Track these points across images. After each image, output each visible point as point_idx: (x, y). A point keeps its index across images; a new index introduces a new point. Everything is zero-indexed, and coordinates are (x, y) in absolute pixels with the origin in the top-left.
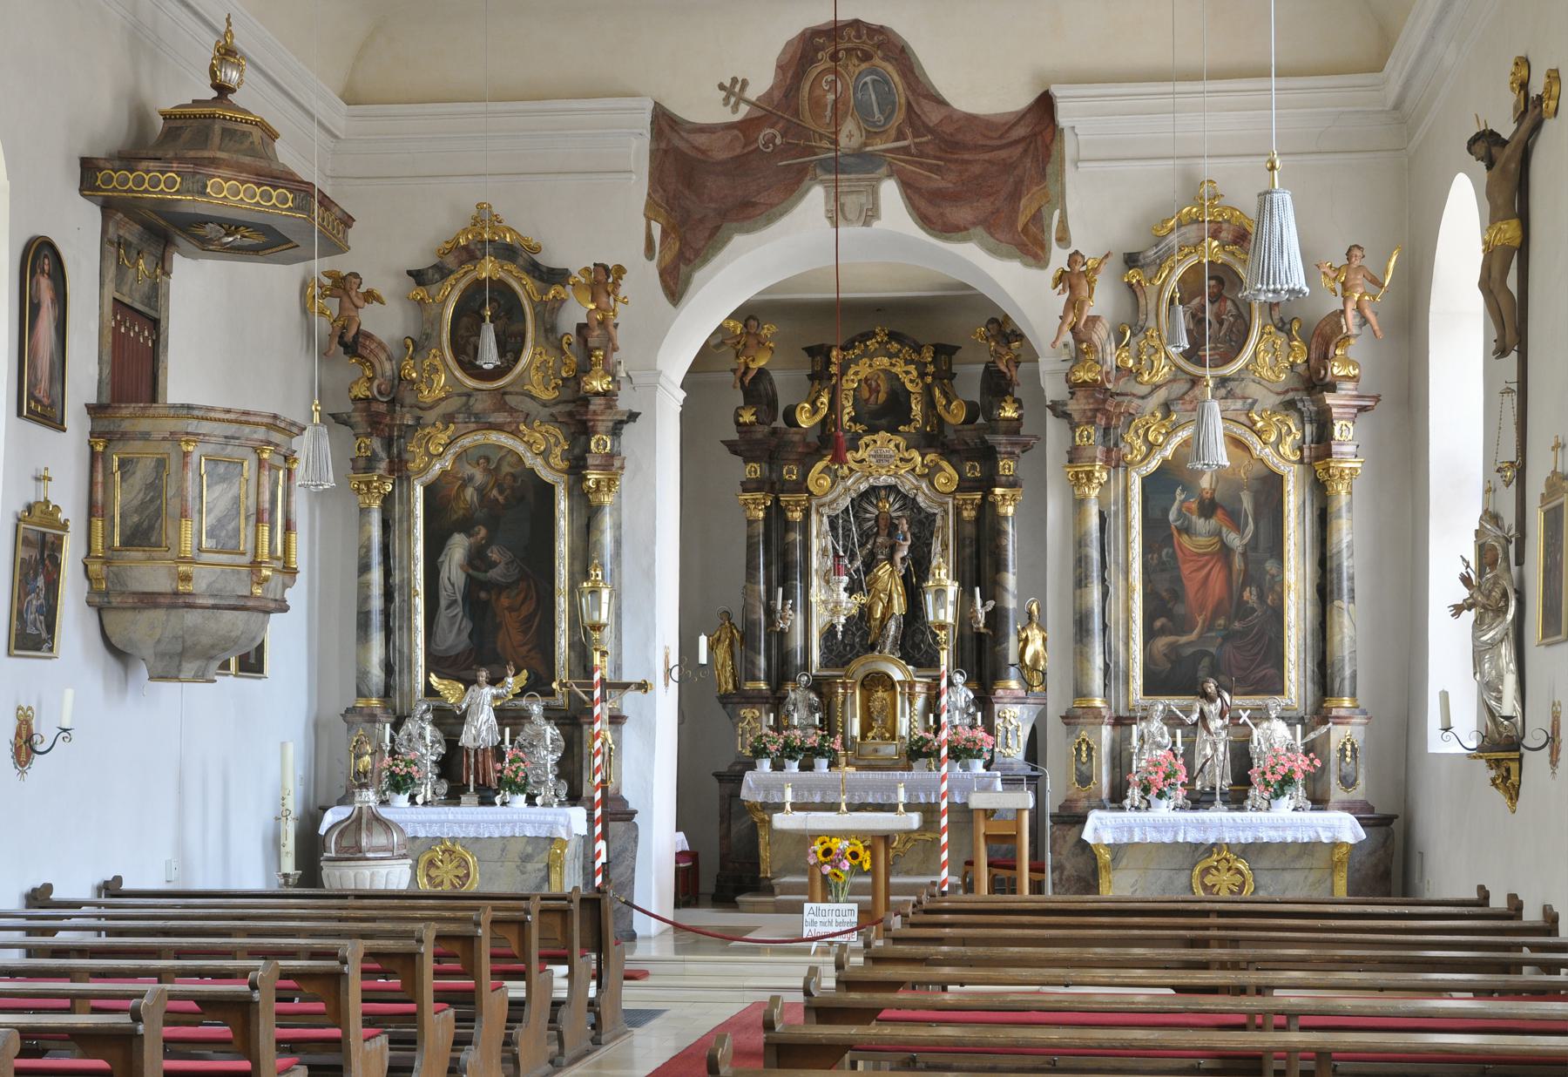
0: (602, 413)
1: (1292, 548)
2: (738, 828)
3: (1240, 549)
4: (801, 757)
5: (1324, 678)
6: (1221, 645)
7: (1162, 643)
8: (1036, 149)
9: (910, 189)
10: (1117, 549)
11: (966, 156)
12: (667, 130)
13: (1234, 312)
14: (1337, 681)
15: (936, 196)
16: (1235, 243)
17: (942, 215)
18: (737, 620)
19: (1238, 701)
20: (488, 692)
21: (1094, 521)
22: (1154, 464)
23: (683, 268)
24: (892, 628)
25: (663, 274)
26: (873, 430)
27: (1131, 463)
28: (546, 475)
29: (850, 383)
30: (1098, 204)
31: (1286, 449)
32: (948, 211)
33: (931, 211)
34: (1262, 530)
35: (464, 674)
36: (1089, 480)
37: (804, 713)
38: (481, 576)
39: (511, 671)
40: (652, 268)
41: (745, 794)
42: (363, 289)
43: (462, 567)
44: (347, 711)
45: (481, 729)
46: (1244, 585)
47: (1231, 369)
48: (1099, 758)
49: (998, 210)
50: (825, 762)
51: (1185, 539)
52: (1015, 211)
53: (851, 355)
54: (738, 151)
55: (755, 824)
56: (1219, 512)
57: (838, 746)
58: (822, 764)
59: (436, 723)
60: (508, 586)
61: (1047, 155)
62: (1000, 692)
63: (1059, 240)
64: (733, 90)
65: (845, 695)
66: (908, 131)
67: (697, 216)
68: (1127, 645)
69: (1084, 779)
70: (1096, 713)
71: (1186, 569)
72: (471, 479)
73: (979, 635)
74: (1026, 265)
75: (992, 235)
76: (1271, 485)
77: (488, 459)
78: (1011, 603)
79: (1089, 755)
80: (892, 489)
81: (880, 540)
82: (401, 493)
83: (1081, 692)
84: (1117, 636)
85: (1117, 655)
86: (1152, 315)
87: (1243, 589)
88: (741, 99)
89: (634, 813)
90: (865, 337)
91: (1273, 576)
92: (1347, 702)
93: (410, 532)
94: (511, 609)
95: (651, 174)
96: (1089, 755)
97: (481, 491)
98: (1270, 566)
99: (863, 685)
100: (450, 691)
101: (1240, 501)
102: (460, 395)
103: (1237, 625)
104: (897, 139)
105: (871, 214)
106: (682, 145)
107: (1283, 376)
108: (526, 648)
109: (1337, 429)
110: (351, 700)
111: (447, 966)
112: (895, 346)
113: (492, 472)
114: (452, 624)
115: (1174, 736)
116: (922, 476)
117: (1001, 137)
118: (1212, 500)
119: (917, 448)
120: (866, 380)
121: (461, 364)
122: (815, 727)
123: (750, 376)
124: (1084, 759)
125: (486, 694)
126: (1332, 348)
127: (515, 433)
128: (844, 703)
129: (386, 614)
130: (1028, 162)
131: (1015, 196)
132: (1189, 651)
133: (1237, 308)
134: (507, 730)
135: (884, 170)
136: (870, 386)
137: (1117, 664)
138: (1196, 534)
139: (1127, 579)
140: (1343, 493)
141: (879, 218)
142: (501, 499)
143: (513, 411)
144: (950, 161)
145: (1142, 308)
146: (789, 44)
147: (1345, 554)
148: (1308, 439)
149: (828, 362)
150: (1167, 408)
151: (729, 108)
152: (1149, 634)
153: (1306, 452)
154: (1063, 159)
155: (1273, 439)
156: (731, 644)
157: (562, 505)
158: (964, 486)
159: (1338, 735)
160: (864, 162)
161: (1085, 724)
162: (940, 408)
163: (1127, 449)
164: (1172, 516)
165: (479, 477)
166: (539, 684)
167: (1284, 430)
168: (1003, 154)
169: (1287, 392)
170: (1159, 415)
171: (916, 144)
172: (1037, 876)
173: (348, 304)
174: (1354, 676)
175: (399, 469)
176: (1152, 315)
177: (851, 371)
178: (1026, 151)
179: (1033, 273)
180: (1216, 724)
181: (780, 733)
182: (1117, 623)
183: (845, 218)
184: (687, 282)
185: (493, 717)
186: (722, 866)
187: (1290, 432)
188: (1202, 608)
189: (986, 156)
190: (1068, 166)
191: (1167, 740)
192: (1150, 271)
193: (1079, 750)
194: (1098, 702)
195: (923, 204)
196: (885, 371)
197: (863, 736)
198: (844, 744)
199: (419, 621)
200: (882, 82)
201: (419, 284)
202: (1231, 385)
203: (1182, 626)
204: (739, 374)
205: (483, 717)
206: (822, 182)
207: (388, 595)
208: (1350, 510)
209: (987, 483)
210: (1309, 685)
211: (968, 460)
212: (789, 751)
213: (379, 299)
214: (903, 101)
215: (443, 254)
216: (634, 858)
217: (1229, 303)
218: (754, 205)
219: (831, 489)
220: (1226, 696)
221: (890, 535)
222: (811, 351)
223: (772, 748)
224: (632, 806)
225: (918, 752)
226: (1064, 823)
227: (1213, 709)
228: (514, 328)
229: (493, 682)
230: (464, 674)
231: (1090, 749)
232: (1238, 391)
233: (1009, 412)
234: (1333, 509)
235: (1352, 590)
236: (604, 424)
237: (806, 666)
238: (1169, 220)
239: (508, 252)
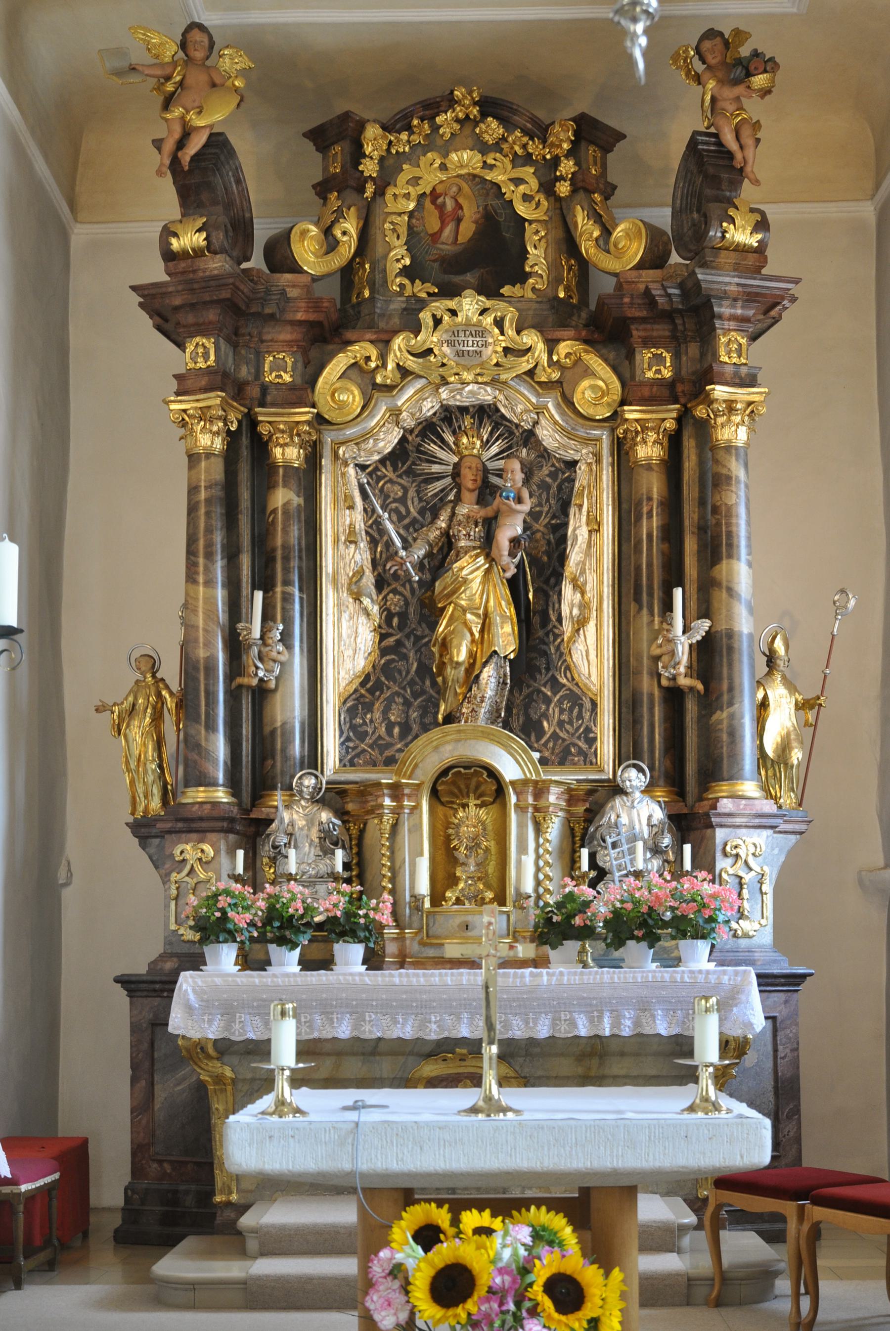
2: (169, 1090)
4: (304, 940)
18: (171, 672)
24: (489, 676)
26: (450, 291)
29: (401, 201)
37: (309, 850)
41: (179, 1022)
50: (357, 951)
53: (403, 142)
55: (201, 1087)
57: (385, 917)
58: (350, 956)
62: (726, 805)
65: (397, 811)
73: (674, 696)
78: (744, 624)
80: (485, 413)
81: (463, 510)
90: (432, 108)
99: (434, 793)
112: (492, 129)
116: (548, 386)
119: (539, 327)
120: (434, 195)
122: (335, 877)
128: (395, 827)
136: (441, 208)
149: (358, 154)
156: (158, 717)
162: (587, 248)
177: (402, 178)
181: (257, 888)
186: (137, 1171)
197: (437, 898)
198: (395, 914)
204: (169, 146)
209: (689, 390)
212: (280, 927)
219: (362, 405)
221: (481, 501)
222: (321, 137)
223: (240, 919)
225: (557, 928)
233: (741, 234)
237: (313, 759)
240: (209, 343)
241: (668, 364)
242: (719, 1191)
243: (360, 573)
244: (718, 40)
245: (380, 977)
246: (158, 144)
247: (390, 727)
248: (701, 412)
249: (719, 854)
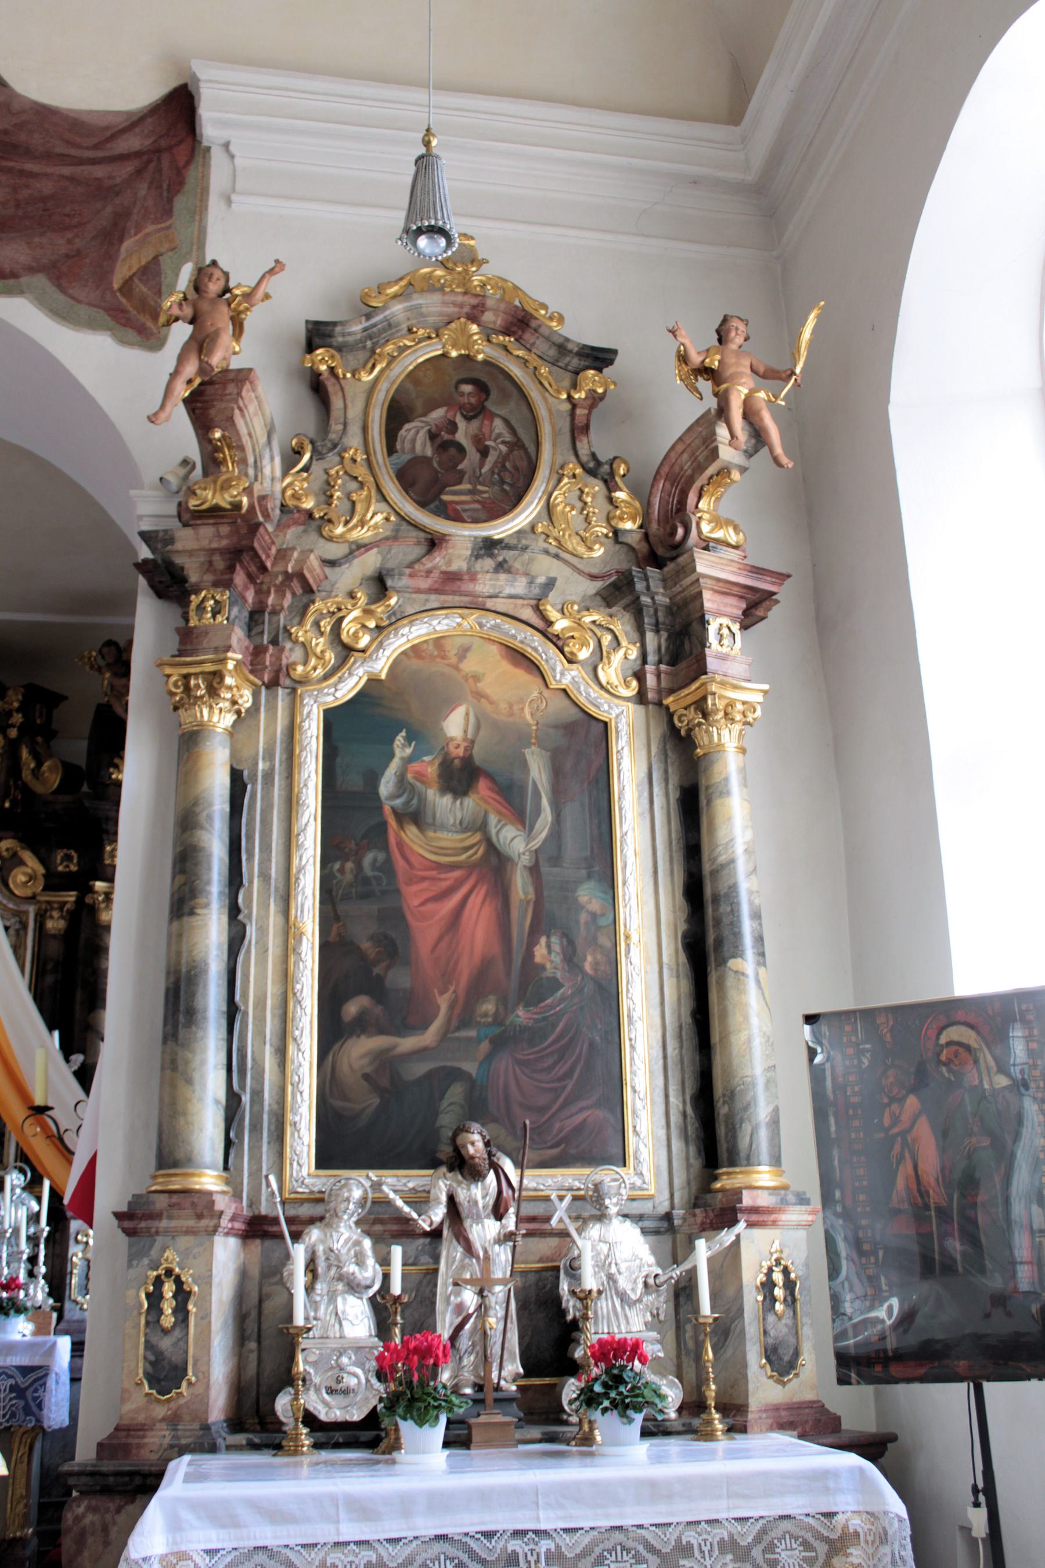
3: (526, 860)
6: (490, 1057)
7: (359, 1050)
8: (159, 171)
10: (266, 848)
11: (30, 166)
13: (508, 437)
14: (747, 1128)
16: (507, 332)
19: (542, 1180)
27: (304, 681)
31: (612, 672)
36: (213, 692)
46: (535, 932)
48: (205, 1316)
49: (79, 253)
51: (411, 833)
52: (111, 256)
56: (482, 785)
61: (177, 183)
68: (281, 1052)
69: (166, 1374)
70: (201, 1205)
71: (413, 896)
74: (123, 342)
75: (63, 290)
76: (583, 743)
79: (181, 1312)
83: (170, 1154)
84: (260, 1033)
86: (355, 429)
87: (532, 943)
91: (594, 916)
92: (764, 1176)
96: (181, 1312)
98: (588, 896)
101: (524, 765)
103: (521, 1015)
109: (712, 629)
115: (384, 1261)
117: (96, 147)
124: (168, 1320)
130: (142, 189)
131: (113, 235)
132: (419, 1069)
137: (257, 1095)
138: (435, 826)
139: (286, 912)
148: (652, 658)
150: (380, 585)
153: (651, 681)
154: (205, 191)
155: (584, 654)
158: (54, 882)
159: (758, 1249)
161: (173, 1234)
162: (26, 775)
163: (298, 654)
164: (386, 787)
167: (607, 639)
168: (99, 172)
174: (775, 1123)
179: (135, 357)
180: (484, 1231)
182: (261, 1003)
188: (448, 976)
189: (66, 171)
190: (215, 204)
193: (155, 1298)
194: (209, 1180)
202: (502, 555)
203: (405, 1015)
210: (677, 1145)
211: (61, 847)
217: (498, 425)
220: (508, 1165)
226: (107, 1491)
227: (479, 1194)
231: (182, 1295)
235: (759, 940)
238: (390, 284)
241: (75, 861)
244: (113, 648)
248: (88, 900)
249: (72, 1242)
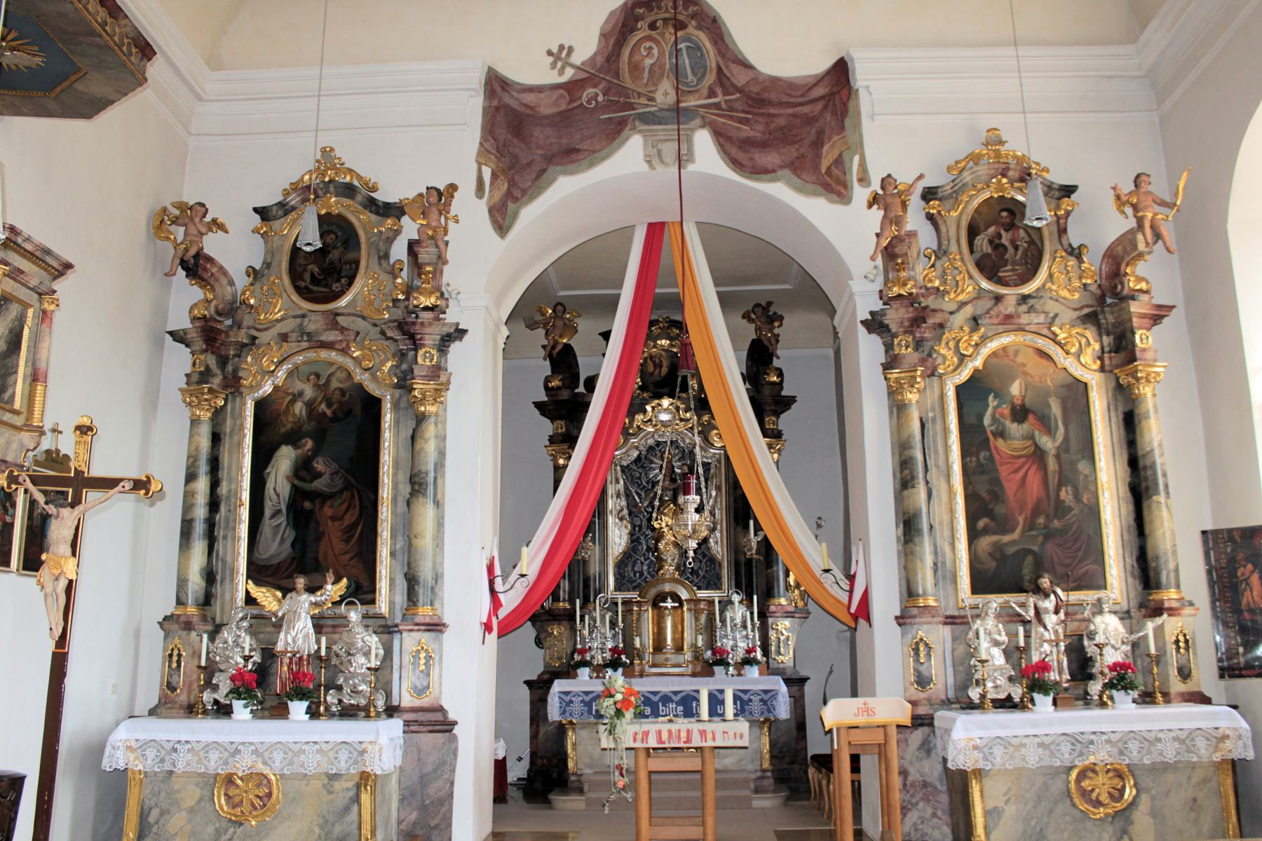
0: (430, 324)
1: (1102, 449)
3: (1053, 452)
5: (1146, 571)
6: (1043, 544)
7: (985, 542)
9: (720, 136)
10: (936, 453)
11: (772, 111)
12: (499, 90)
13: (1027, 239)
15: (746, 144)
17: (751, 159)
19: (1075, 596)
20: (305, 599)
21: (916, 426)
22: (965, 375)
23: (511, 206)
25: (491, 211)
28: (373, 389)
30: (902, 136)
31: (1087, 358)
32: (756, 156)
33: (741, 156)
34: (1072, 433)
35: (284, 583)
38: (306, 486)
39: (330, 577)
40: (482, 206)
42: (208, 219)
43: (288, 478)
44: (166, 618)
45: (298, 636)
46: (1060, 484)
47: (1027, 289)
51: (1000, 442)
52: (818, 156)
54: (564, 107)
56: (1031, 417)
59: (252, 631)
60: (332, 496)
62: (772, 608)
63: (860, 180)
64: (560, 56)
66: (719, 91)
67: (525, 161)
68: (953, 545)
71: (1003, 471)
72: (301, 394)
73: (749, 562)
74: (831, 201)
75: (799, 177)
76: (1076, 393)
77: (318, 376)
82: (233, 409)
85: (944, 556)
86: (953, 242)
88: (567, 64)
89: (454, 723)
91: (1086, 476)
93: (240, 445)
94: (334, 519)
95: (484, 128)
97: (310, 405)
100: (267, 598)
101: (1049, 406)
102: (295, 317)
104: (709, 97)
105: (681, 161)
106: (512, 103)
107: (1077, 296)
108: (348, 556)
110: (170, 607)
111: (412, 728)
113: (322, 387)
114: (275, 534)
117: (802, 96)
118: (1023, 406)
121: (298, 289)
123: (557, 350)
125: (303, 604)
126: (1123, 266)
127: (345, 351)
129: (211, 525)
130: (828, 116)
131: (818, 144)
132: (1011, 550)
133: (1029, 236)
134: (324, 640)
135: (698, 121)
136: (654, 363)
138: (1010, 438)
140: (1149, 395)
141: (693, 161)
142: (329, 412)
143: (343, 330)
144: (758, 114)
145: (944, 235)
146: (612, 13)
147: (1157, 453)
151: (556, 72)
152: (973, 535)
153: (1107, 362)
155: (1073, 350)
157: (388, 418)
160: (678, 114)
161: (920, 623)
164: (987, 421)
165: (309, 392)
166: (363, 591)
167: (1083, 341)
168: (806, 109)
169: (1082, 308)
170: (966, 329)
171: (726, 101)
172: (855, 776)
173: (193, 230)
175: (233, 385)
176: (953, 242)
178: (825, 107)
180: (1051, 620)
183: (662, 162)
184: (515, 216)
185: (310, 625)
187: (1089, 344)
188: (1022, 507)
189: (790, 111)
191: (1003, 638)
192: (949, 203)
194: (932, 603)
195: (734, 151)
196: (667, 351)
199: (243, 530)
200: (696, 48)
201: (263, 219)
202: (1032, 302)
203: (1004, 526)
204: (549, 349)
205: (299, 625)
206: (640, 132)
207: (214, 505)
208: (1156, 412)
213: (222, 227)
214: (714, 65)
215: (286, 193)
216: (453, 771)
217: (1021, 231)
218: (577, 151)
220: (1059, 591)
224: (452, 716)
227: (1049, 604)
228: (351, 256)
229: (311, 590)
230: (284, 583)
232: (1038, 307)
234: (1140, 410)
235: (1166, 486)
236: (431, 338)
239: (348, 191)
240: (563, 423)
242: (645, 227)
243: (622, 510)
245: (318, 724)
246: (544, 347)
247: (635, 573)
